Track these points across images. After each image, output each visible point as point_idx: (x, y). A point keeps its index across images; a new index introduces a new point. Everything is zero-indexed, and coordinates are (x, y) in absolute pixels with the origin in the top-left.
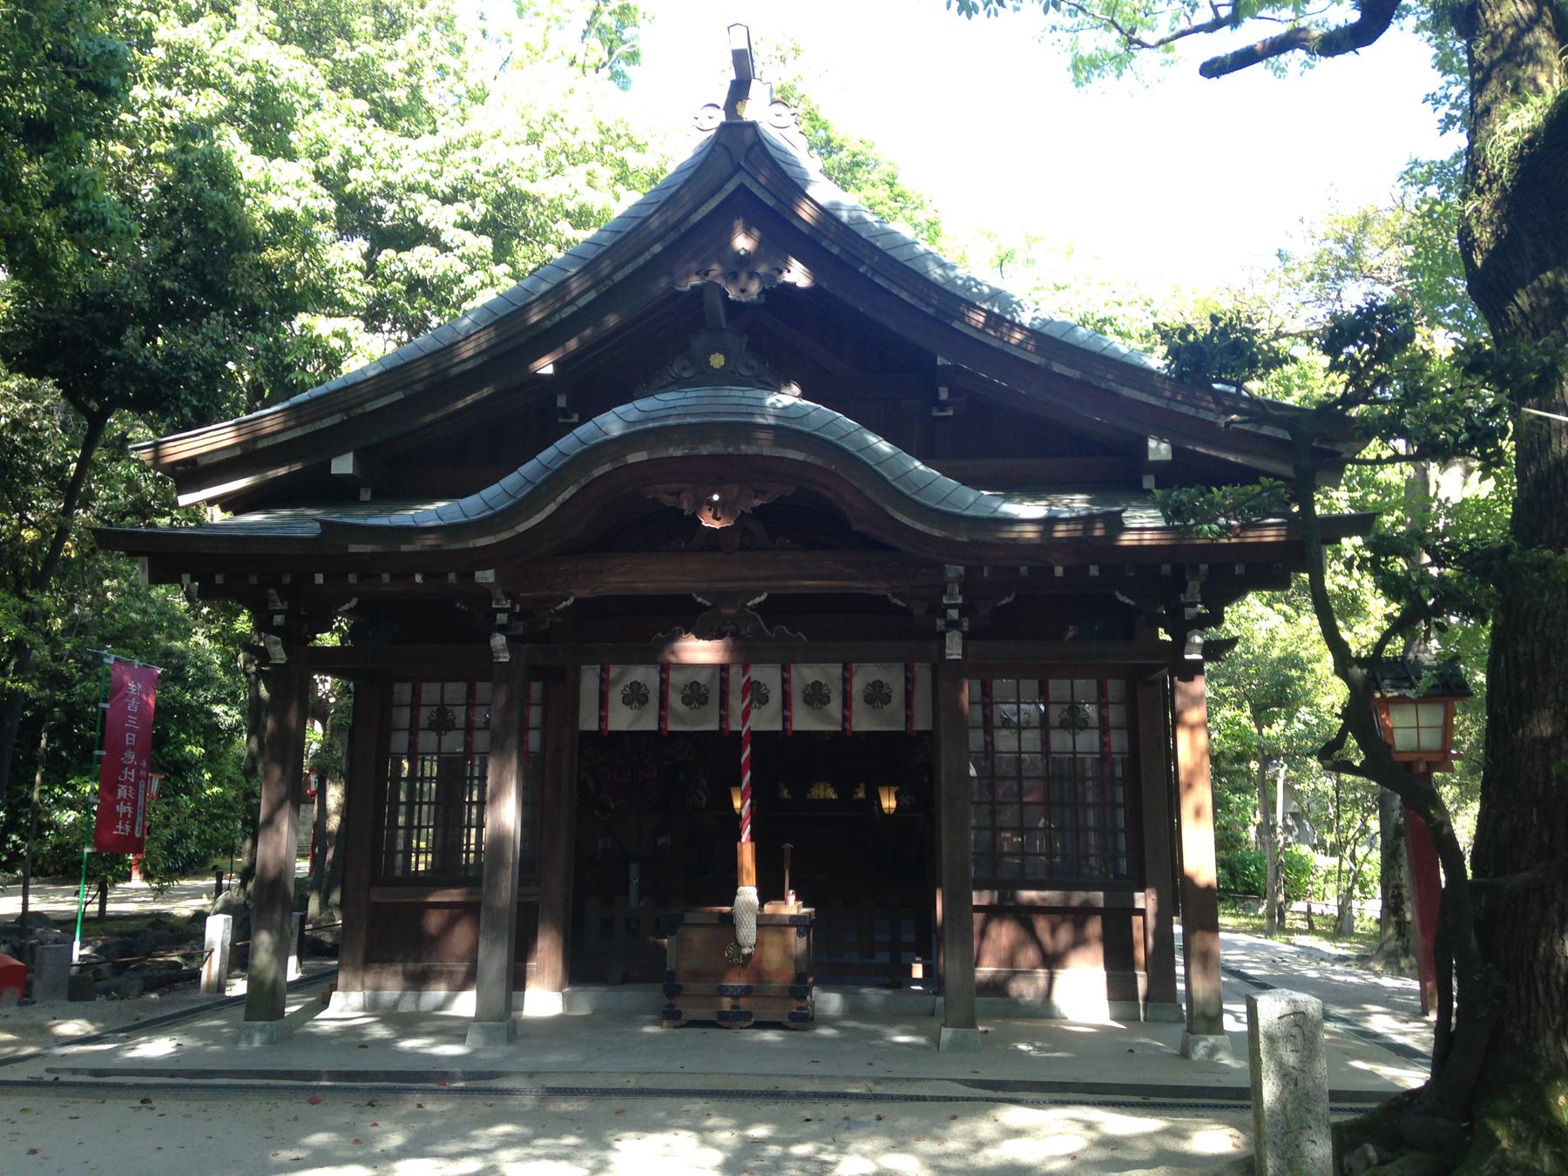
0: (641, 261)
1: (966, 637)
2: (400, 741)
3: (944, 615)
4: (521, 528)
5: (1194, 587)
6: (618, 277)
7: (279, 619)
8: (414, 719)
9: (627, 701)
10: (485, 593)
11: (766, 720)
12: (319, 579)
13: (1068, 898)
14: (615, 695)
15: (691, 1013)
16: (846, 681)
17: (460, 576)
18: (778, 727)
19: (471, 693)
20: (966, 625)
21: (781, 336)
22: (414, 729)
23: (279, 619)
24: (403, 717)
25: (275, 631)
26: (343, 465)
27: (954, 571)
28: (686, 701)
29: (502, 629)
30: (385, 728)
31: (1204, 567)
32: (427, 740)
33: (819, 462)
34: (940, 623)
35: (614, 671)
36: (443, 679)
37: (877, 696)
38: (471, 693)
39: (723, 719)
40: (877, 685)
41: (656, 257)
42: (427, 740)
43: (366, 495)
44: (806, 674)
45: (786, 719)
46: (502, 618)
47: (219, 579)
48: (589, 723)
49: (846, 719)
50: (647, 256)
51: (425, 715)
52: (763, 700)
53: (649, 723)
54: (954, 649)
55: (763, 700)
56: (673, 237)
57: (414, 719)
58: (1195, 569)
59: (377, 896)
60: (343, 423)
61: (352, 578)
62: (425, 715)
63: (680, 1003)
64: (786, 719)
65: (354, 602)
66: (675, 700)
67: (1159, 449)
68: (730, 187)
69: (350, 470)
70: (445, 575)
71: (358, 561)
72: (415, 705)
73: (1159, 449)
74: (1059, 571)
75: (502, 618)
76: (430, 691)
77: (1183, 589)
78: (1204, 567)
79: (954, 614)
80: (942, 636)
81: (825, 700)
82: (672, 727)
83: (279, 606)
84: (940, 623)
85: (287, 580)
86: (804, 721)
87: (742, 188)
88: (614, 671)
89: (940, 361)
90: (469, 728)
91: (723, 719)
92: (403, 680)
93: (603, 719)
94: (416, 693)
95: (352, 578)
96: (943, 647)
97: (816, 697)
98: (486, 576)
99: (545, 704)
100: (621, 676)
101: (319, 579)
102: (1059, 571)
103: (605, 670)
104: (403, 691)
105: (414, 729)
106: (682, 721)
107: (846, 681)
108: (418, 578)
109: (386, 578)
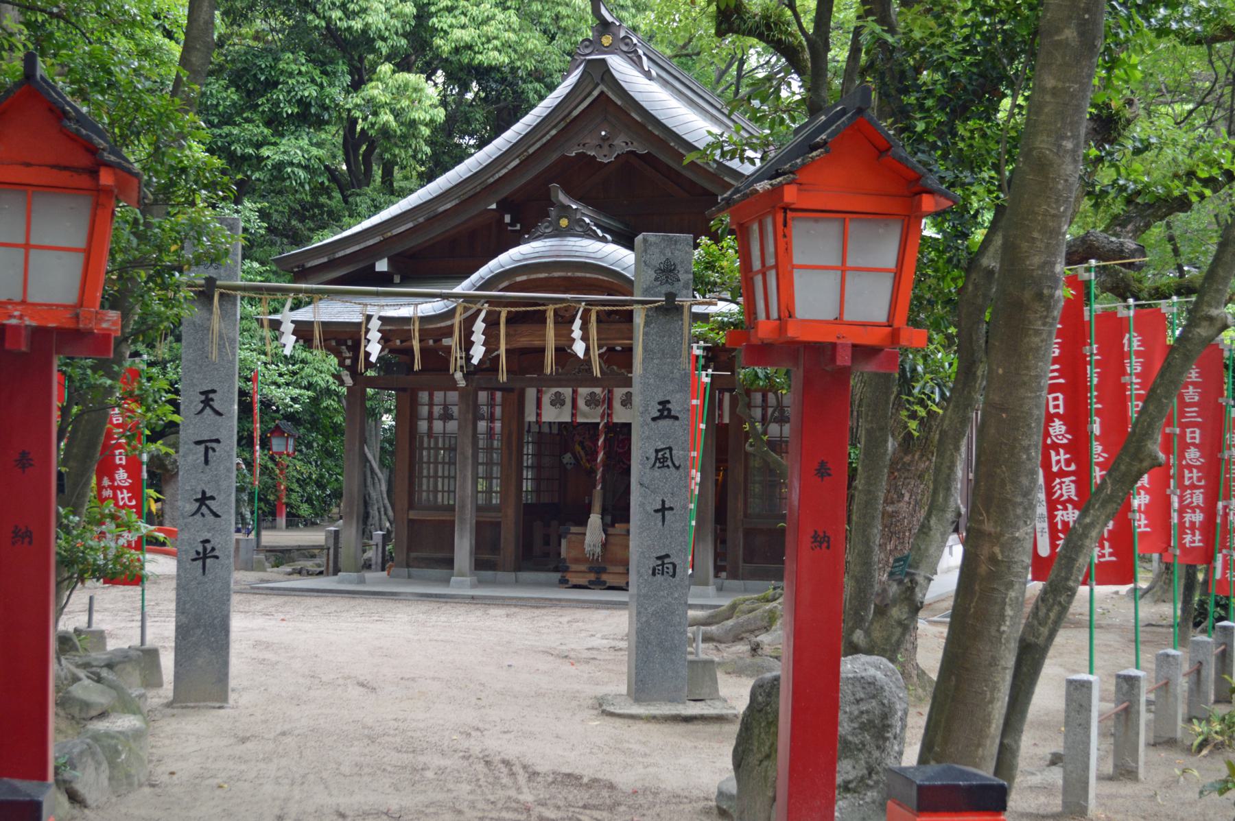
0: (544, 140)
6: (531, 151)
8: (431, 413)
9: (553, 403)
13: (496, 492)
14: (546, 400)
15: (574, 580)
17: (435, 342)
24: (424, 411)
26: (382, 266)
28: (588, 403)
41: (553, 137)
43: (397, 279)
48: (530, 417)
50: (548, 137)
51: (437, 410)
53: (567, 418)
56: (562, 125)
57: (431, 413)
59: (413, 515)
62: (437, 410)
63: (568, 576)
66: (581, 403)
68: (596, 93)
69: (385, 269)
72: (431, 404)
76: (439, 396)
82: (580, 420)
85: (350, 343)
87: (602, 93)
92: (423, 389)
93: (539, 415)
94: (431, 396)
104: (424, 396)
105: (430, 418)
106: (585, 416)
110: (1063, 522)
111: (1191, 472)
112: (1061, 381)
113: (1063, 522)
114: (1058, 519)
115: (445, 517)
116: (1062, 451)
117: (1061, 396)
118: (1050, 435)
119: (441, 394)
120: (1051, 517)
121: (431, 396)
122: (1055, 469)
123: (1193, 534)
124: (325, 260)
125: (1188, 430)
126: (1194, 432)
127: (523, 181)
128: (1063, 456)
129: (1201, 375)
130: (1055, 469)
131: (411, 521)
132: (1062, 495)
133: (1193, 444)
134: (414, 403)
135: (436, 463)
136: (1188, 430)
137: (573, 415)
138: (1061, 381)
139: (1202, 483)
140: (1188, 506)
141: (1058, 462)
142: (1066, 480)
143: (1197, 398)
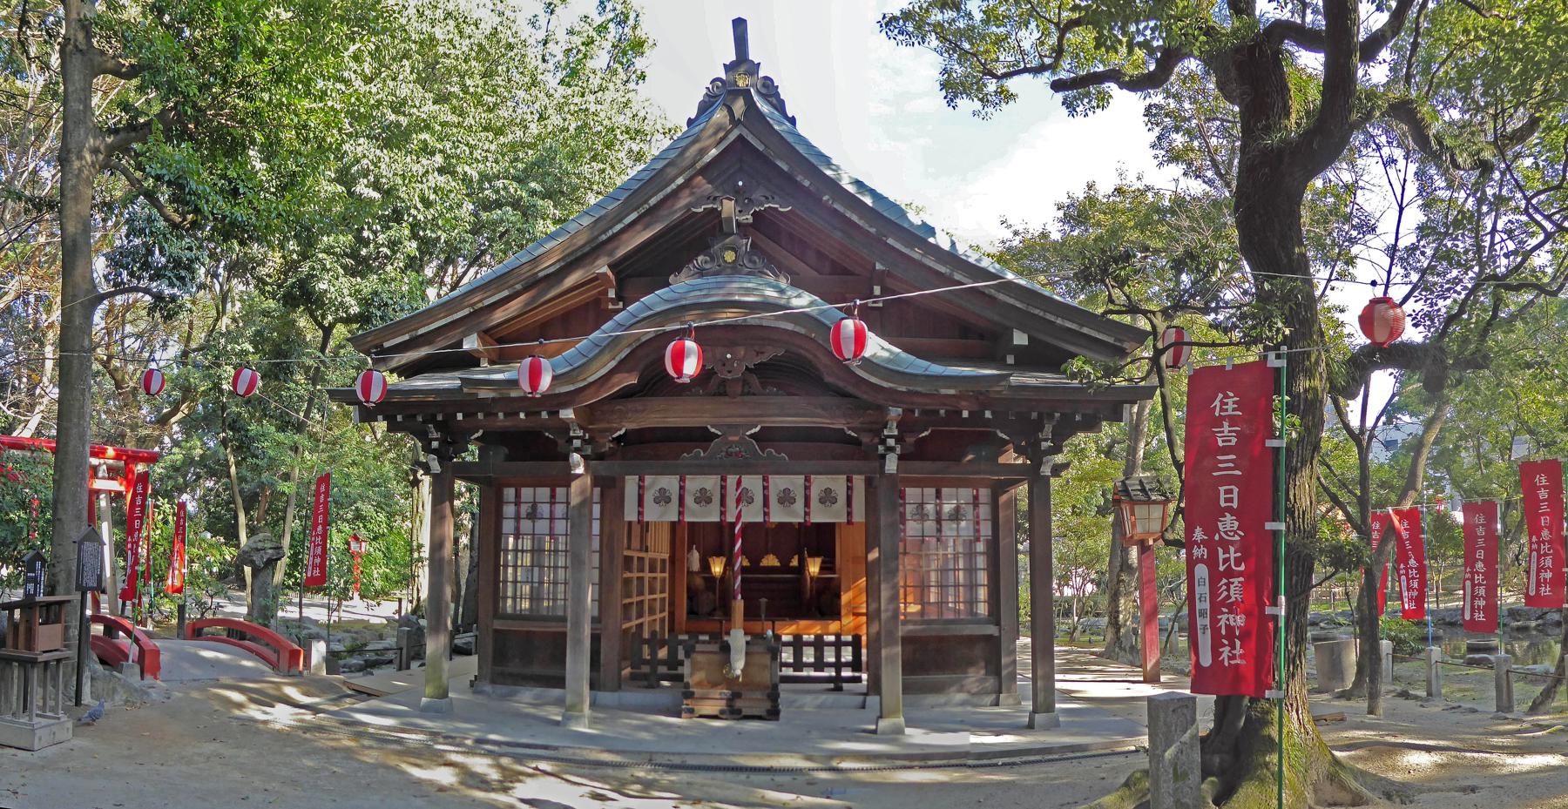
1: (901, 458)
2: (508, 526)
3: (883, 442)
4: (1059, 321)
5: (1048, 429)
7: (435, 444)
9: (657, 501)
10: (565, 427)
11: (752, 515)
12: (460, 416)
14: (649, 497)
16: (807, 488)
17: (550, 413)
18: (760, 519)
19: (553, 496)
20: (898, 450)
21: (771, 241)
22: (518, 518)
23: (435, 444)
24: (509, 510)
25: (434, 451)
27: (895, 412)
28: (697, 501)
29: (577, 450)
30: (499, 517)
31: (1057, 415)
32: (526, 525)
33: (803, 331)
34: (881, 448)
35: (648, 479)
36: (535, 485)
37: (828, 498)
38: (553, 496)
39: (723, 513)
40: (828, 491)
42: (526, 525)
44: (778, 482)
45: (766, 514)
46: (577, 443)
47: (399, 418)
49: (807, 514)
51: (524, 509)
52: (709, 501)
54: (891, 465)
55: (751, 501)
57: (518, 513)
58: (1051, 416)
59: (498, 625)
60: (471, 314)
61: (480, 416)
62: (524, 509)
64: (766, 514)
65: (480, 433)
66: (689, 500)
67: (1020, 339)
68: (732, 137)
70: (539, 413)
71: (484, 405)
72: (518, 503)
73: (1020, 339)
74: (965, 414)
75: (577, 443)
76: (527, 493)
77: (1041, 429)
78: (1057, 415)
79: (891, 442)
80: (883, 457)
81: (793, 501)
83: (436, 435)
84: (881, 448)
85: (440, 418)
86: (778, 516)
87: (740, 138)
88: (648, 479)
89: (879, 266)
90: (552, 519)
91: (723, 513)
92: (509, 486)
93: (640, 513)
94: (518, 495)
95: (480, 416)
96: (883, 466)
97: (786, 498)
98: (568, 414)
99: (602, 502)
100: (654, 483)
101: (460, 416)
102: (965, 414)
103: (641, 480)
104: (510, 493)
106: (694, 515)
107: (807, 488)
108: (522, 416)
109: (501, 415)
110: (1228, 627)
111: (1226, 551)
112: (1238, 473)
113: (1228, 627)
114: (1222, 623)
115: (554, 628)
116: (1232, 549)
117: (1236, 490)
118: (1218, 531)
119: (531, 490)
120: (1214, 621)
121: (518, 495)
122: (1222, 568)
123: (1233, 647)
124: (406, 337)
125: (1222, 489)
126: (1230, 492)
127: (924, 340)
128: (1233, 555)
129: (1239, 406)
130: (1222, 568)
131: (496, 631)
132: (1229, 597)
133: (1230, 510)
134: (500, 502)
135: (556, 567)
136: (1222, 489)
137: (681, 513)
138: (1238, 473)
139: (1242, 568)
140: (1223, 603)
141: (1226, 560)
142: (1236, 580)
143: (1234, 440)
